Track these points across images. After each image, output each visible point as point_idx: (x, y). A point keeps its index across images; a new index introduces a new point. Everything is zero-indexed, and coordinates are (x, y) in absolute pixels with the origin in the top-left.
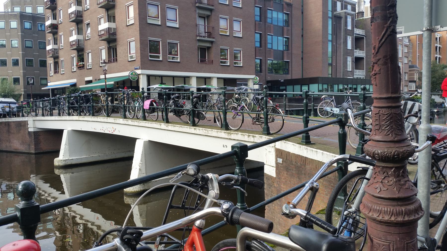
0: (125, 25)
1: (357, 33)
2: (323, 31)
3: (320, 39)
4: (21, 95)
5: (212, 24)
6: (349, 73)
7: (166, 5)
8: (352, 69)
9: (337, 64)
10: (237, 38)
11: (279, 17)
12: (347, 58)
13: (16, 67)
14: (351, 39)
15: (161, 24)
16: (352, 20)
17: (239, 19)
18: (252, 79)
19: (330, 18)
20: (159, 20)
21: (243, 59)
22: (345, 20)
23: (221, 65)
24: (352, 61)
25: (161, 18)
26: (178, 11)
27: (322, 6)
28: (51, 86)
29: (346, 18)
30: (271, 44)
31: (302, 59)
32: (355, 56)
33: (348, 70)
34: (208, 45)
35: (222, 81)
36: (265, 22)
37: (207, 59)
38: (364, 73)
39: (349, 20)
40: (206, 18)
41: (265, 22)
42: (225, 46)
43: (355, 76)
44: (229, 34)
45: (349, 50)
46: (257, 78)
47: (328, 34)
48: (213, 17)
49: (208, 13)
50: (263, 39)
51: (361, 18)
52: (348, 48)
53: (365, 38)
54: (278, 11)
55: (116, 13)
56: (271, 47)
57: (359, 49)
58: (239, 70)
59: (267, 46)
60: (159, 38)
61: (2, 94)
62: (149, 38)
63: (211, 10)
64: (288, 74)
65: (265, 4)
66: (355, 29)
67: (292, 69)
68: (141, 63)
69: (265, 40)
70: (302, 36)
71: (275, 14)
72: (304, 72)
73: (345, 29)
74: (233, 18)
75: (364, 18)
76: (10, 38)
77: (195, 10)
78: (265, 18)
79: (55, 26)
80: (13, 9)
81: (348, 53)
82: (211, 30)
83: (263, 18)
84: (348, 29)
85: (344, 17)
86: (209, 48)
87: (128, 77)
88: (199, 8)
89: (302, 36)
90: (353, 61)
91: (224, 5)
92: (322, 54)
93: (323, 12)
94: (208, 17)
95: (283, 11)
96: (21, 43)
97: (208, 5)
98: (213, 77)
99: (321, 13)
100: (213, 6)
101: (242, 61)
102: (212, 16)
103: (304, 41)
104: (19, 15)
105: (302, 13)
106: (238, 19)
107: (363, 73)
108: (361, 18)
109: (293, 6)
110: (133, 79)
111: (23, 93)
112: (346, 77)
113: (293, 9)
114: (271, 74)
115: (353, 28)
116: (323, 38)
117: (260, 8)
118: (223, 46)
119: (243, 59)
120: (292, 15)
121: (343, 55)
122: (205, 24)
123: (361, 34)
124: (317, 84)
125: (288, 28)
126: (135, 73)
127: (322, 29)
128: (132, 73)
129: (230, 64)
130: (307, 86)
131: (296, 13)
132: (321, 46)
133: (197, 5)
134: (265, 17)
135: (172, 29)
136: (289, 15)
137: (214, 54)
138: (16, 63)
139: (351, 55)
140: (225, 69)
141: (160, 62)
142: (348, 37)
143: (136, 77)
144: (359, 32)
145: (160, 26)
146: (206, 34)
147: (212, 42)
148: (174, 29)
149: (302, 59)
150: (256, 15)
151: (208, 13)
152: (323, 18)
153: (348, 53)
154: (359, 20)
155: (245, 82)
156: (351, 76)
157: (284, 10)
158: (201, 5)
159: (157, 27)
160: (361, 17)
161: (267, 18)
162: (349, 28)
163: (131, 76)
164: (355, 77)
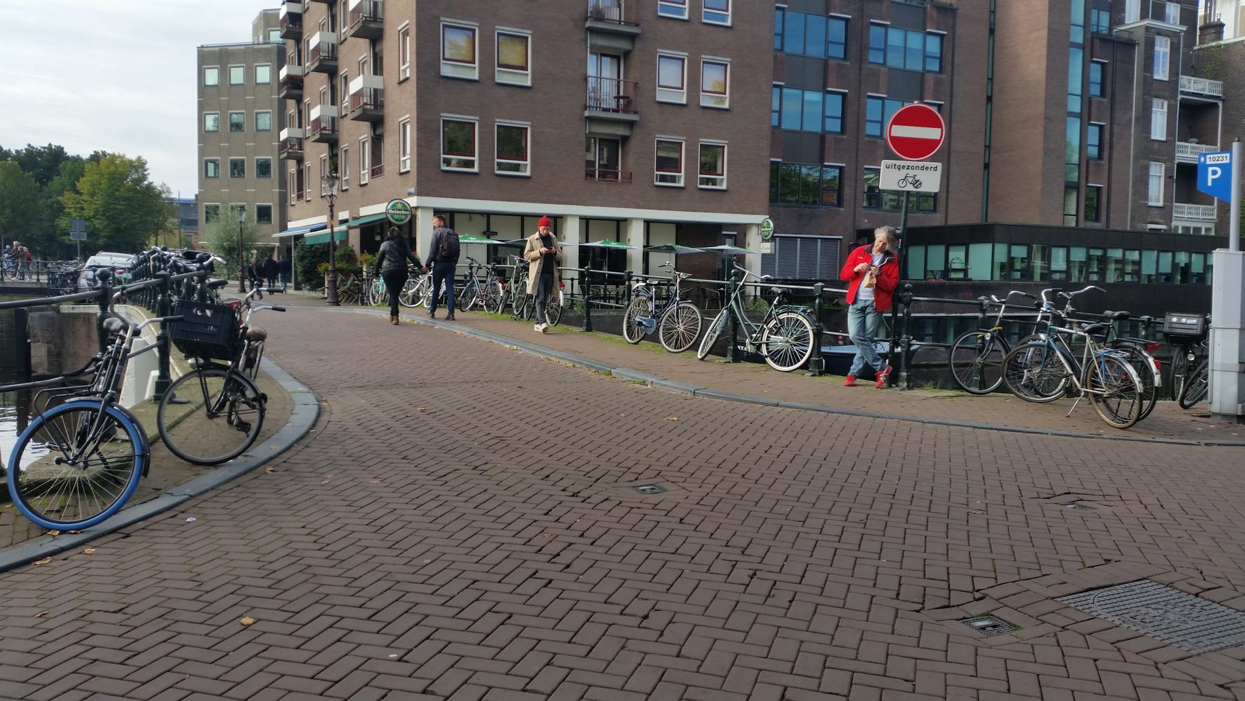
0: (397, 81)
1: (1192, 90)
2: (1047, 84)
3: (1040, 109)
4: (273, 249)
5: (634, 75)
6: (1155, 212)
7: (497, 27)
8: (1164, 201)
9: (1114, 186)
10: (710, 112)
11: (908, 46)
12: (1147, 168)
13: (264, 181)
14: (1165, 109)
15: (480, 77)
16: (1174, 49)
17: (719, 59)
18: (758, 225)
19: (1076, 45)
20: (475, 68)
21: (729, 171)
22: (1145, 50)
23: (657, 186)
24: (1168, 177)
25: (480, 62)
26: (532, 42)
27: (1049, 11)
28: (293, 229)
29: (1150, 45)
30: (879, 125)
31: (987, 166)
32: (1177, 161)
33: (1150, 204)
34: (621, 131)
35: (673, 229)
36: (861, 59)
37: (620, 169)
38: (1213, 214)
39: (1162, 48)
40: (620, 58)
41: (861, 59)
42: (672, 135)
43: (1174, 224)
44: (688, 100)
45: (1156, 144)
46: (769, 224)
47: (1067, 93)
48: (636, 57)
49: (624, 45)
50: (851, 110)
51: (1214, 44)
52: (1153, 137)
53: (1220, 104)
54: (906, 27)
55: (384, 50)
56: (878, 133)
57: (1196, 140)
58: (716, 199)
59: (864, 130)
60: (472, 115)
61: (225, 244)
62: (443, 114)
63: (632, 37)
64: (935, 210)
65: (862, 11)
66: (1181, 76)
67: (947, 197)
68: (418, 179)
69: (859, 113)
70: (989, 99)
71: (895, 37)
72: (990, 208)
73: (1145, 78)
74: (703, 56)
75: (1222, 42)
76: (254, 108)
77: (581, 39)
78: (861, 50)
79: (295, 80)
80: (267, 36)
81: (1152, 151)
82: (631, 94)
83: (853, 49)
84: (1156, 77)
85: (1142, 41)
86: (625, 139)
87: (385, 216)
88: (593, 31)
89: (989, 99)
90: (1171, 177)
91: (672, 22)
92: (1045, 154)
93: (1052, 31)
94: (627, 54)
95: (924, 28)
96: (276, 120)
97: (627, 23)
98: (631, 219)
99: (1044, 33)
100: (637, 25)
101: (728, 174)
102: (636, 53)
103: (995, 115)
104: (276, 51)
105: (992, 32)
106: (719, 58)
107: (1209, 215)
108: (1214, 44)
109: (959, 11)
110: (397, 220)
111: (277, 244)
112: (1140, 226)
113: (959, 20)
114: (873, 212)
115: (1174, 73)
116: (1046, 108)
117: (847, 20)
118: (666, 134)
119: (728, 171)
120: (954, 39)
121: (1136, 158)
122: (619, 77)
123: (1207, 92)
124: (989, 246)
125: (939, 75)
126: (404, 205)
127: (1044, 80)
128: (394, 205)
129: (685, 184)
130: (964, 248)
131: (970, 32)
132: (1041, 130)
133: (588, 24)
134: (861, 45)
135: (510, 90)
136: (945, 39)
137: (630, 160)
138: (264, 168)
139: (1165, 158)
140: (671, 197)
141: (473, 177)
142: (1156, 102)
143: (406, 215)
144: (1193, 85)
145: (477, 84)
146: (621, 101)
147: (631, 124)
148: (518, 90)
149: (987, 166)
150: (831, 42)
151: (624, 45)
152: (1050, 46)
153: (1152, 151)
154: (1204, 49)
155: (739, 234)
156: (1160, 221)
157: (928, 25)
158: (600, 25)
159: (469, 86)
160: (1213, 41)
161: (868, 48)
162: (1161, 73)
163: (391, 212)
164: (1177, 227)
